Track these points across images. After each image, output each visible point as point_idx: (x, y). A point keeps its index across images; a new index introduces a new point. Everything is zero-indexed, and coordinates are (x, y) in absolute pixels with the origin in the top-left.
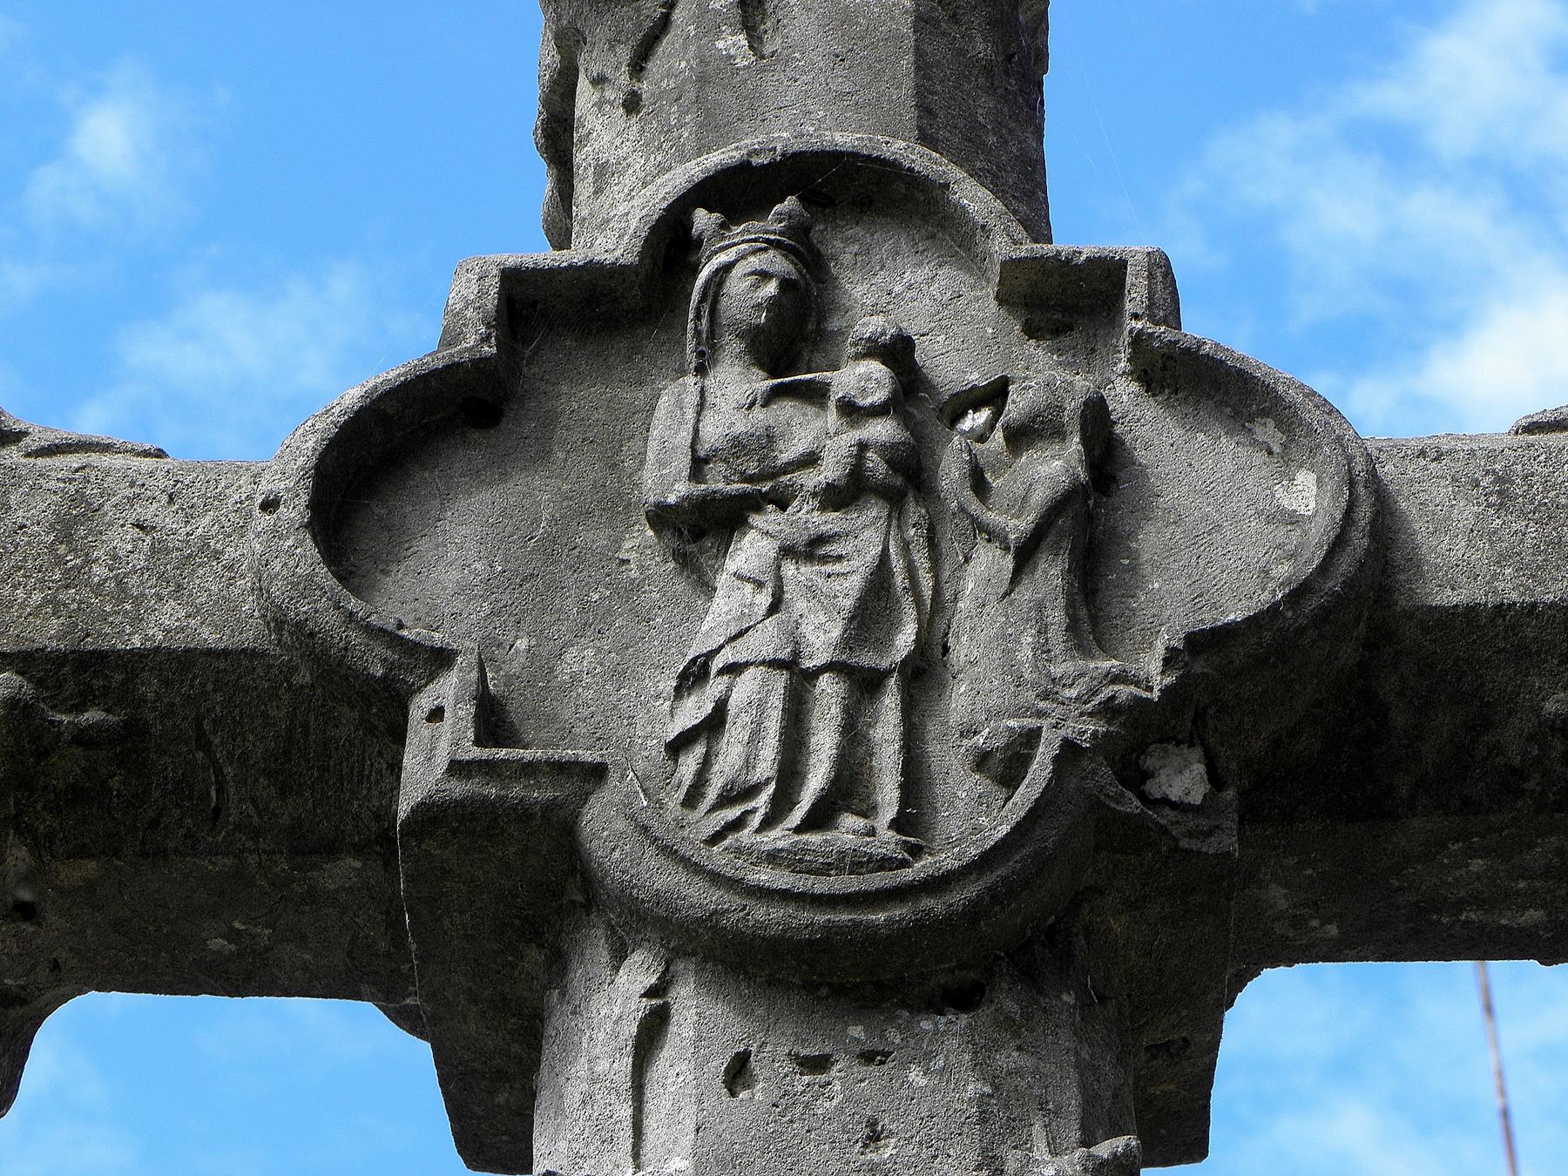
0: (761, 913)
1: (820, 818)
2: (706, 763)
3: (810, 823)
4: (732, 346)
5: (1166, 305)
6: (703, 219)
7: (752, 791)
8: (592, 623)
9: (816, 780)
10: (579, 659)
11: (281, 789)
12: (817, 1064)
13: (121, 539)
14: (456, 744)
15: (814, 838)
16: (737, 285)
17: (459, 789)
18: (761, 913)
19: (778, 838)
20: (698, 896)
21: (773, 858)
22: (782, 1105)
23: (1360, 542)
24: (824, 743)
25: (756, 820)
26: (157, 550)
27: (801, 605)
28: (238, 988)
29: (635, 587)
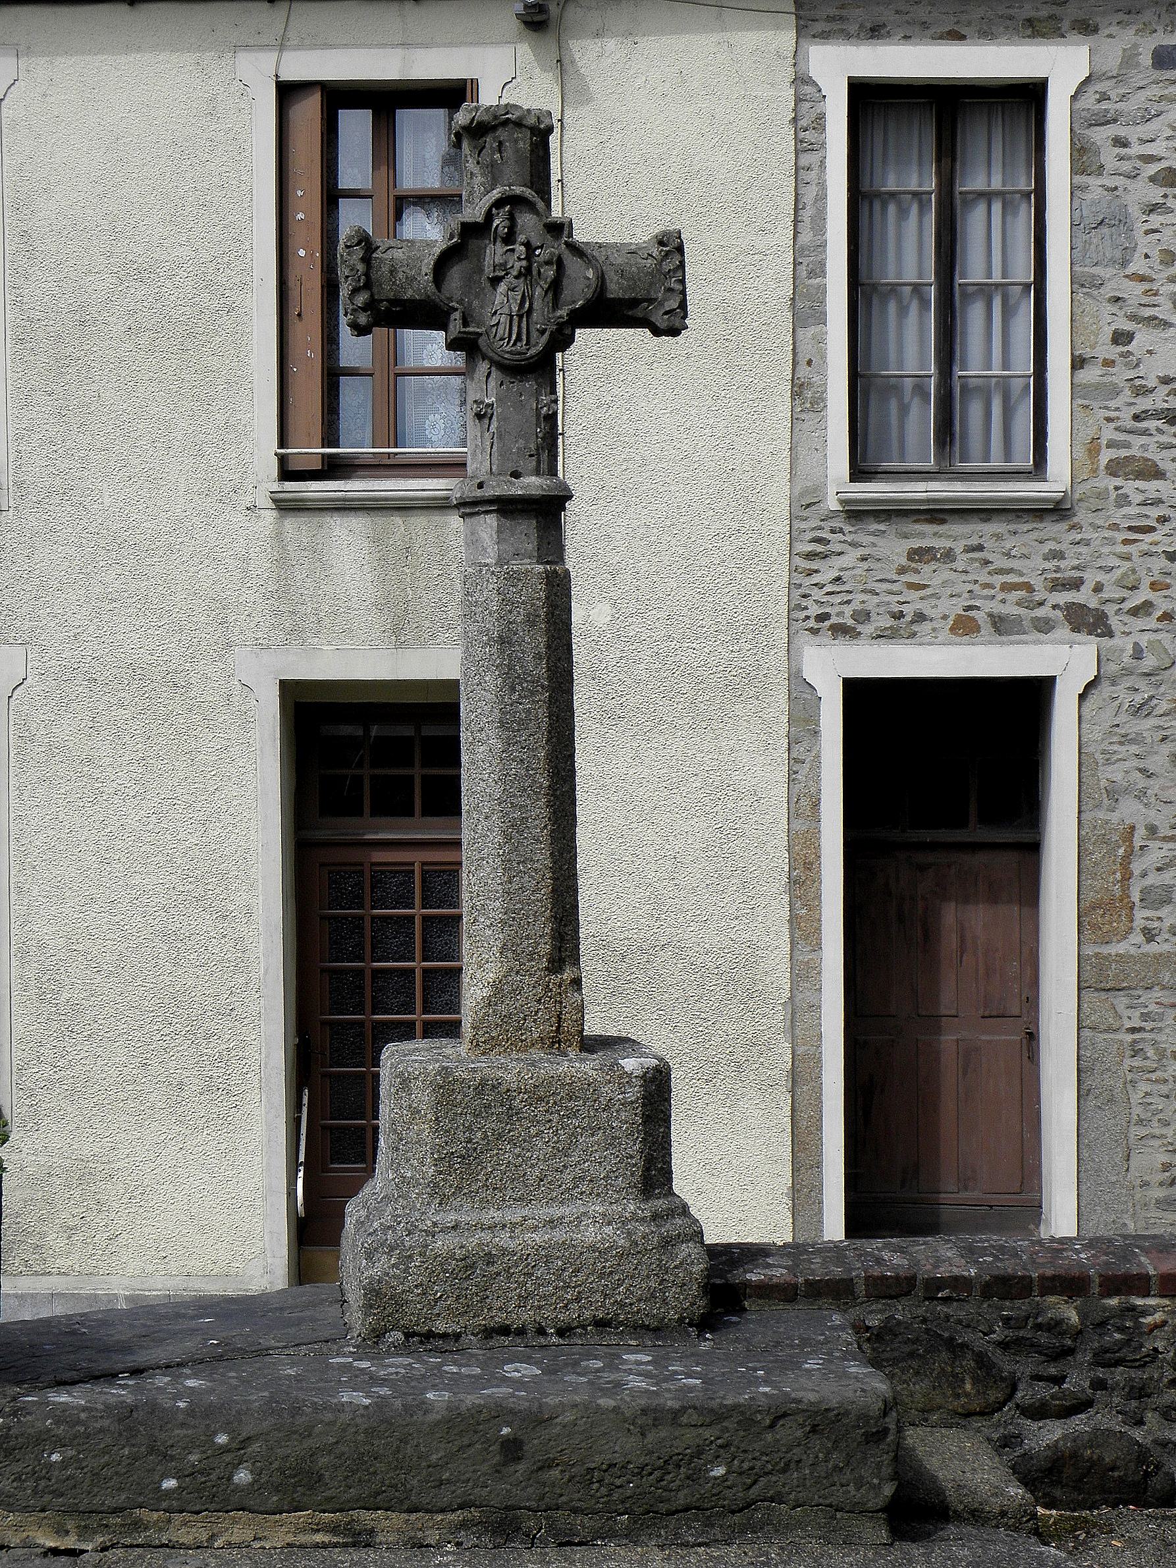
0: (506, 361)
1: (514, 344)
2: (497, 330)
3: (513, 346)
4: (499, 240)
5: (570, 235)
6: (494, 211)
7: (505, 339)
8: (477, 296)
9: (514, 337)
10: (476, 303)
11: (606, 1045)
12: (513, 383)
13: (401, 275)
14: (460, 327)
15: (513, 348)
16: (500, 229)
17: (460, 335)
18: (506, 361)
19: (508, 349)
20: (496, 358)
21: (508, 352)
22: (508, 389)
23: (598, 290)
24: (515, 329)
25: (505, 344)
26: (407, 278)
27: (511, 301)
28: (569, 887)
29: (484, 289)
